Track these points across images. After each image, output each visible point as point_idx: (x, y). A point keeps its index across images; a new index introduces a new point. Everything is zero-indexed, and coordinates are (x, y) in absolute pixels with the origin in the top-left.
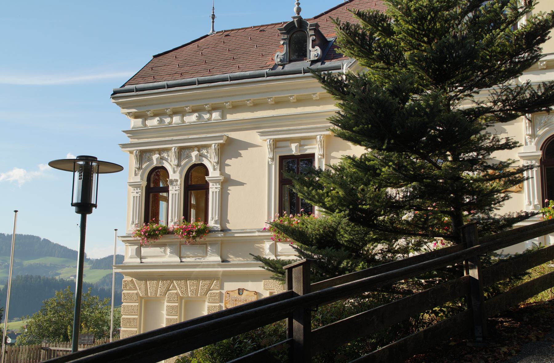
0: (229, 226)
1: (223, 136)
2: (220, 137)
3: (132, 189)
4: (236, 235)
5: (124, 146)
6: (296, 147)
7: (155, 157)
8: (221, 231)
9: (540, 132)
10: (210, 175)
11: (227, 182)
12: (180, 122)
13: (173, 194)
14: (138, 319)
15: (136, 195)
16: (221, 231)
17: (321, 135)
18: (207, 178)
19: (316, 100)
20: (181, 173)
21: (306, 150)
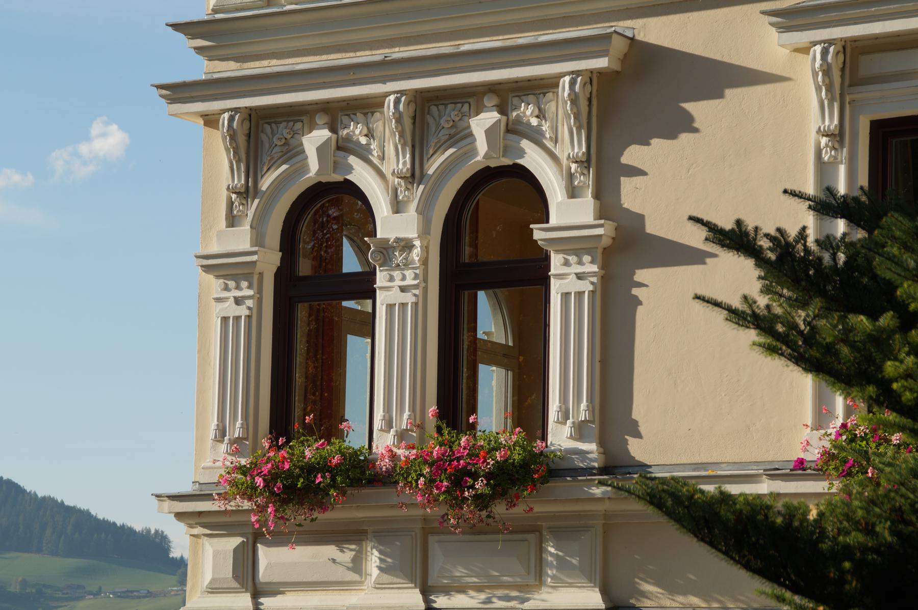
1: (606, 37)
5: (178, 92)
10: (553, 221)
13: (566, 296)
18: (539, 234)
20: (424, 210)
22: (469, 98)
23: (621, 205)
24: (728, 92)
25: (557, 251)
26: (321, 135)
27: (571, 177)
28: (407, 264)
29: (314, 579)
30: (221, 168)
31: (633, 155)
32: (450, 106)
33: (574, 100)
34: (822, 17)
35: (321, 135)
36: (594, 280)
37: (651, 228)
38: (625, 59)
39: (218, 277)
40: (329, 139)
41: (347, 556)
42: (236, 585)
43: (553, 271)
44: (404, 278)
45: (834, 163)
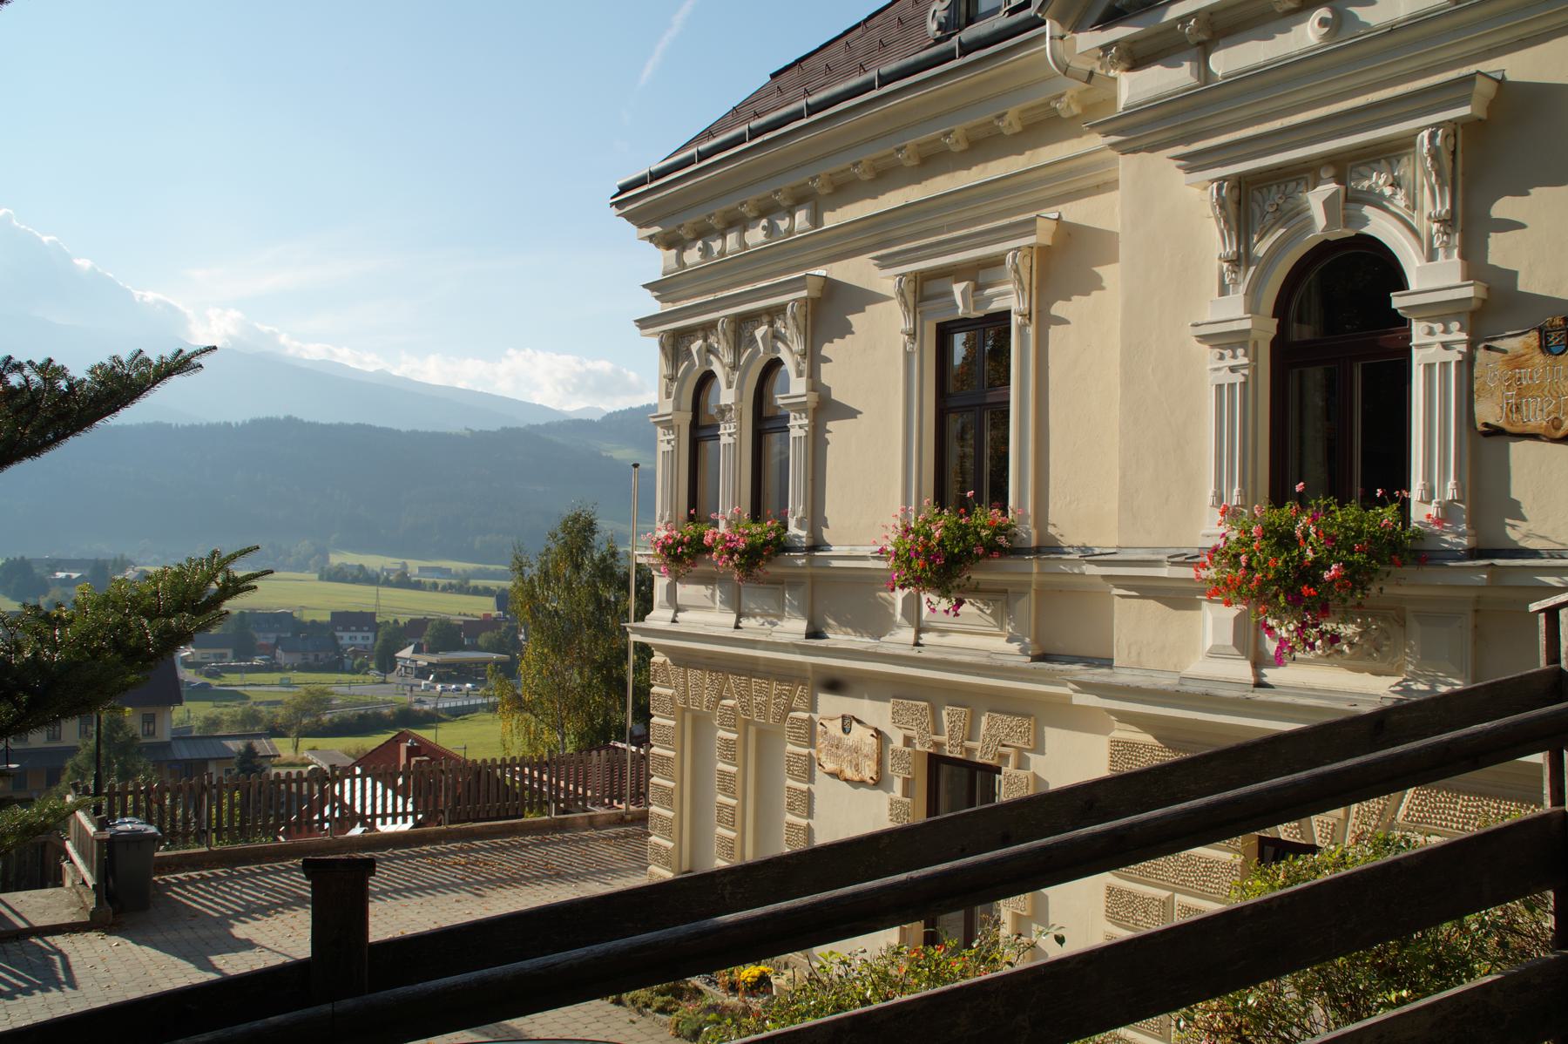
0: (1516, 534)
1: (1469, 80)
2: (799, 284)
3: (1209, 354)
4: (835, 563)
5: (644, 323)
6: (963, 293)
7: (1317, 199)
8: (1474, 553)
9: (1261, 248)
10: (1413, 284)
11: (825, 408)
12: (1193, 81)
13: (1429, 367)
14: (739, 779)
15: (1227, 378)
16: (1474, 553)
17: (1018, 249)
18: (1398, 301)
19: (1016, 135)
20: (740, 388)
21: (990, 299)
22: (1305, 173)
25: (1418, 319)
26: (1328, 188)
28: (730, 421)
30: (1214, 241)
31: (1503, 208)
32: (1274, 188)
33: (1435, 154)
34: (897, 259)
35: (1328, 188)
36: (1246, 372)
37: (835, 396)
38: (1492, 105)
39: (1213, 346)
40: (1336, 193)
43: (1415, 341)
44: (1234, 357)
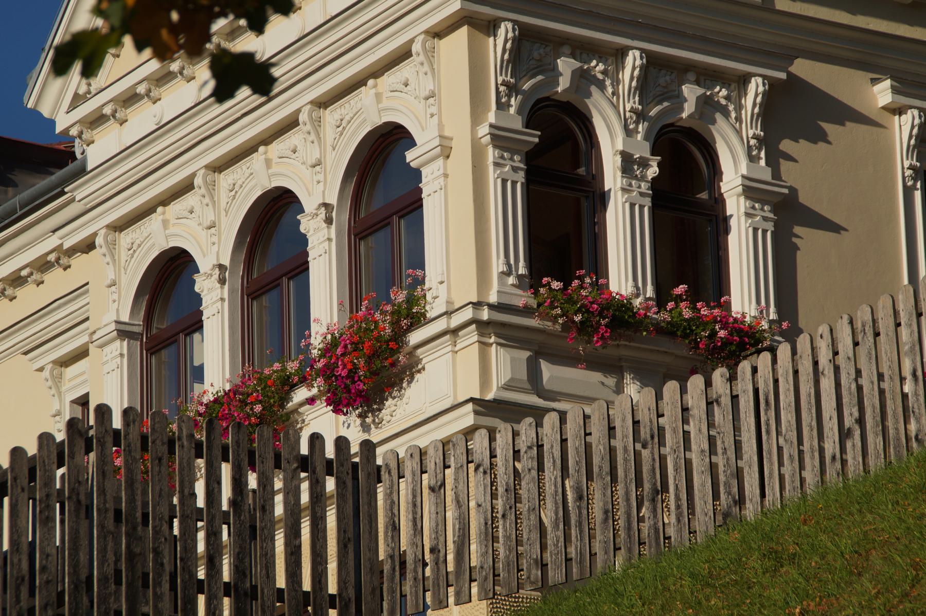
23: (109, 47)
24: (848, 124)
27: (749, 148)
28: (643, 178)
29: (582, 394)
41: (611, 381)
42: (528, 386)
45: (914, 187)
